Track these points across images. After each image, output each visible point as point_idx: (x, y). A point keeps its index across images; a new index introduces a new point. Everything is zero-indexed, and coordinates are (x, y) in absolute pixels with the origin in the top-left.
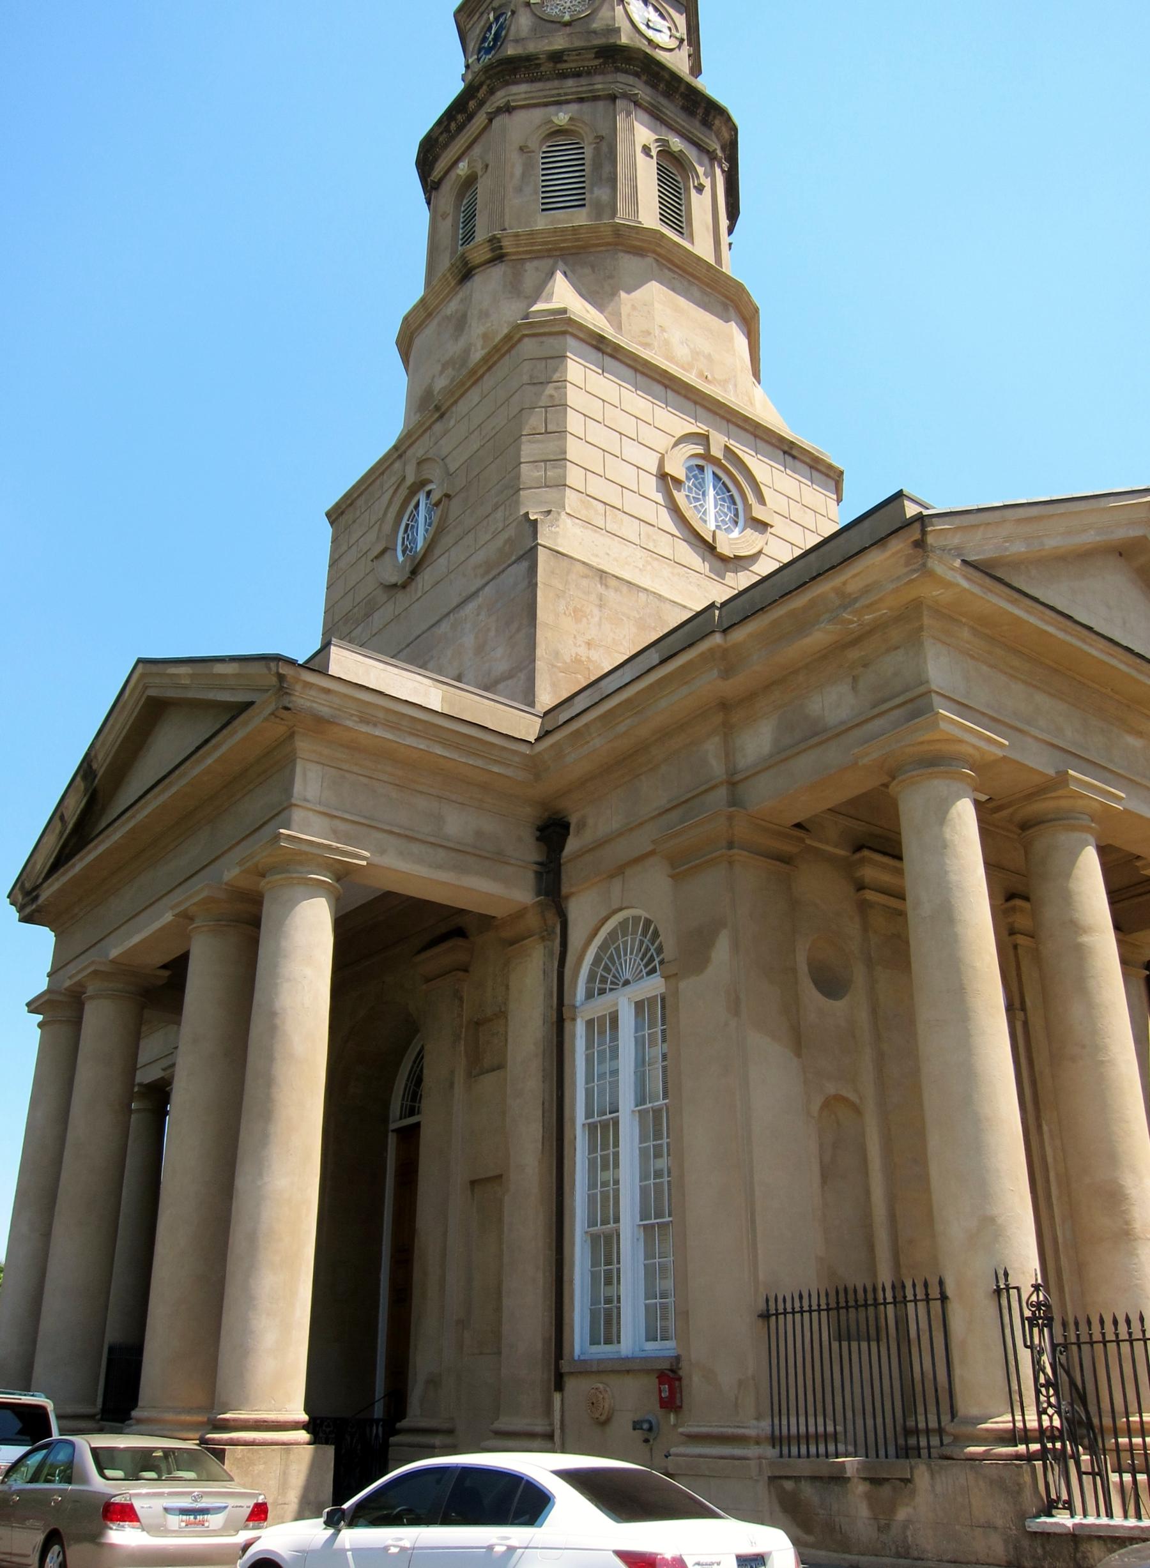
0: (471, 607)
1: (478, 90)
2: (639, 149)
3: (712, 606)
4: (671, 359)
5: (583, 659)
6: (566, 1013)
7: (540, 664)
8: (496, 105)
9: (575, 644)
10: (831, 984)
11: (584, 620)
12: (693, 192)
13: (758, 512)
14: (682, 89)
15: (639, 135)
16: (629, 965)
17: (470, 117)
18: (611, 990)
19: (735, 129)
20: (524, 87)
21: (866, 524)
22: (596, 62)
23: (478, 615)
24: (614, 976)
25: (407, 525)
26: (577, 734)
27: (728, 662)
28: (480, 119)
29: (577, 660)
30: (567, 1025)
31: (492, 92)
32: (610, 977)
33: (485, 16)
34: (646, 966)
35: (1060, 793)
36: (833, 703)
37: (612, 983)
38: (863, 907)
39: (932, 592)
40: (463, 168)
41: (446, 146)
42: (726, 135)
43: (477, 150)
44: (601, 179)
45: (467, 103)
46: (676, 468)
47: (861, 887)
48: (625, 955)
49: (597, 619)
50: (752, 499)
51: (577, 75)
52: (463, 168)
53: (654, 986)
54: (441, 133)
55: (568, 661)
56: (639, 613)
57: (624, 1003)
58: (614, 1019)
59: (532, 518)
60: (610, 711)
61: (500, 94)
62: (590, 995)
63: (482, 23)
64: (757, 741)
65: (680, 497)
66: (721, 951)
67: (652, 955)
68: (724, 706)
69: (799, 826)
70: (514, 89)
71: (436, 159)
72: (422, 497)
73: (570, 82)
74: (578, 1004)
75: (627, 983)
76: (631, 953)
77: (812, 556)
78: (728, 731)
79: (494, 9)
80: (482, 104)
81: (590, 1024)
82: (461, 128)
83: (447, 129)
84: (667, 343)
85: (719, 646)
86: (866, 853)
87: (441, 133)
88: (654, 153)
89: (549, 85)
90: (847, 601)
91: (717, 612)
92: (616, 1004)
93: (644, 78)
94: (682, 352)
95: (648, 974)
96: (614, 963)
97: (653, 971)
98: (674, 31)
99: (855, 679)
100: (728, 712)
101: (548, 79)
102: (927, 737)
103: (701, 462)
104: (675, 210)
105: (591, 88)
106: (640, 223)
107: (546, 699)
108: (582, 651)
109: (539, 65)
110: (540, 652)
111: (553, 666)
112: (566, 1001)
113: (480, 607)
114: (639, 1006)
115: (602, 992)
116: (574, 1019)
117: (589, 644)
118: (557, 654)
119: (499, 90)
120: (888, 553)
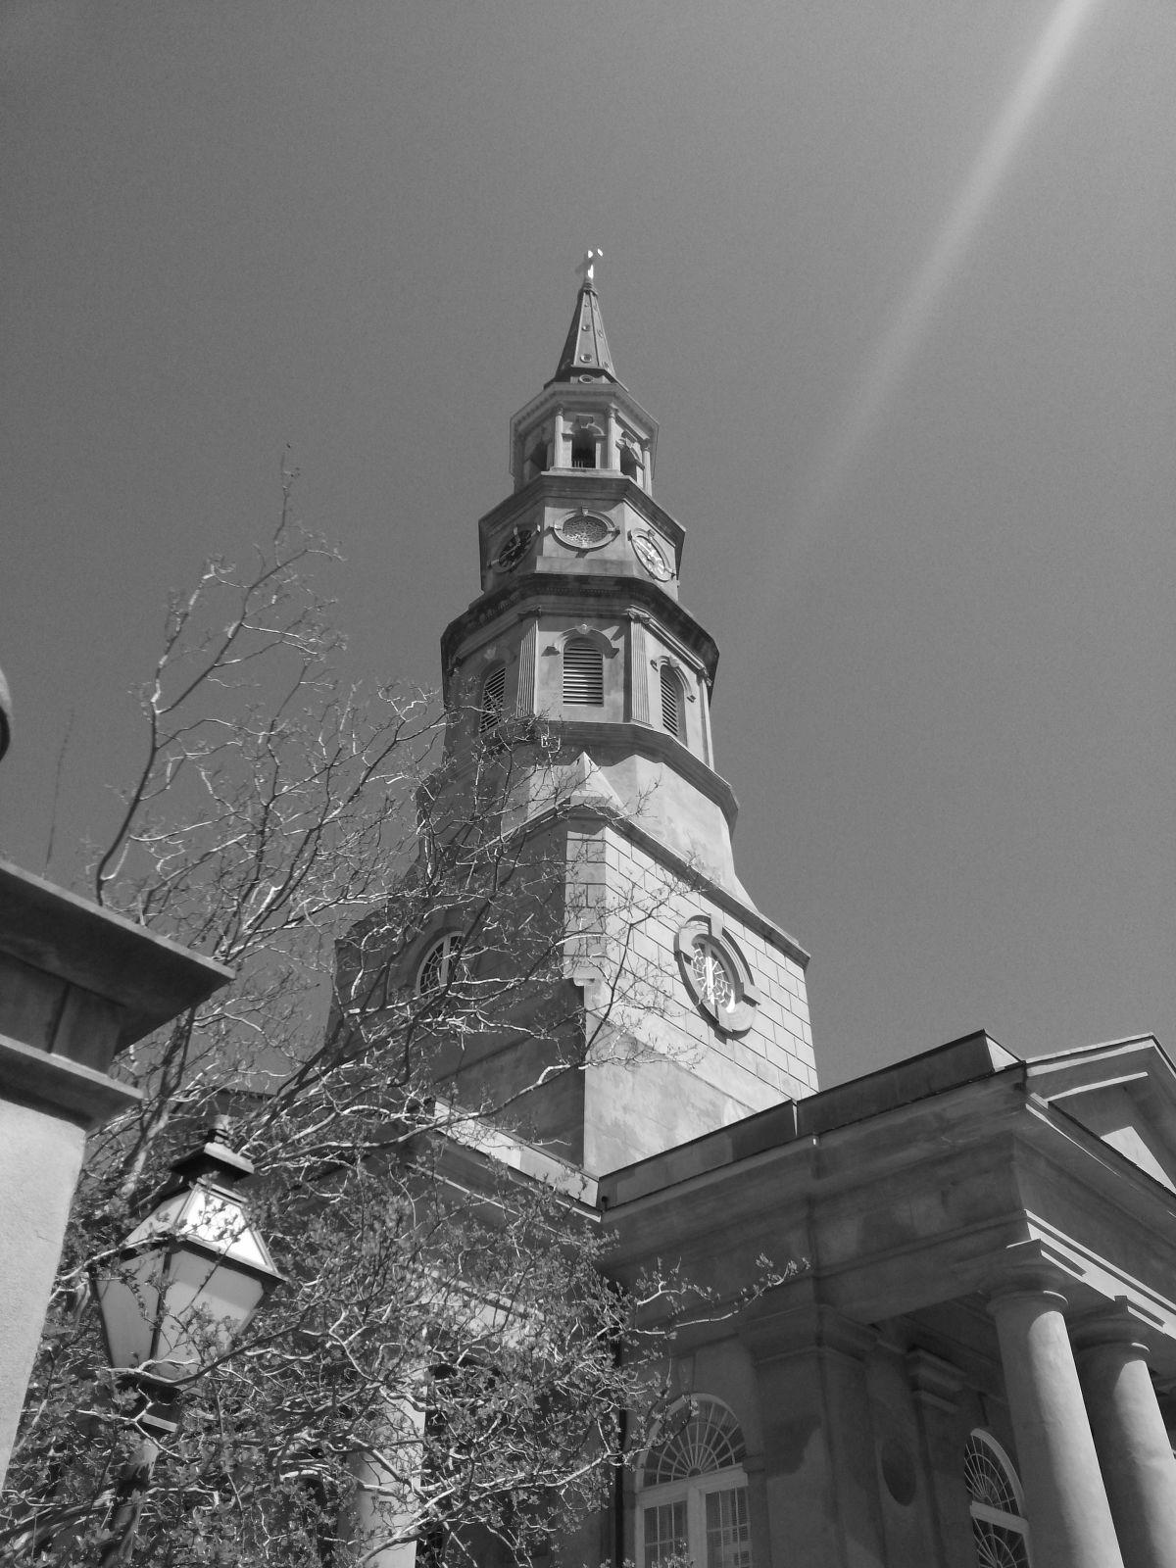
0: (508, 1059)
1: (511, 593)
2: (648, 663)
3: (789, 1103)
4: (676, 846)
5: (622, 1123)
6: (626, 1498)
7: (587, 1126)
8: (528, 609)
9: (614, 1108)
10: (902, 1491)
11: (621, 1085)
12: (686, 700)
13: (749, 991)
14: (681, 618)
15: (649, 648)
16: (698, 1451)
17: (500, 613)
18: (676, 1478)
19: (717, 654)
20: (552, 599)
21: (949, 1054)
22: (616, 588)
23: (517, 1067)
24: (680, 1463)
25: (428, 966)
26: (655, 1210)
27: (820, 1164)
28: (510, 617)
29: (616, 1124)
30: (627, 1512)
31: (523, 597)
32: (675, 1464)
33: (508, 529)
34: (719, 1456)
35: (1118, 1316)
36: (922, 1212)
37: (677, 1470)
38: (918, 1406)
39: (1023, 1128)
40: (490, 654)
41: (472, 631)
42: (710, 657)
43: (504, 641)
44: (617, 685)
45: (499, 601)
46: (687, 948)
47: (915, 1386)
48: (693, 1441)
49: (631, 1084)
50: (743, 977)
51: (598, 595)
52: (490, 654)
53: (734, 1478)
54: (470, 621)
55: (609, 1124)
56: (662, 1080)
57: (694, 1493)
58: (680, 1510)
59: (578, 984)
60: (696, 1193)
61: (531, 600)
62: (650, 1481)
63: (505, 534)
64: (843, 1239)
65: (689, 968)
66: (815, 1450)
67: (726, 1446)
68: (811, 1201)
69: (873, 1325)
70: (544, 598)
71: (461, 640)
72: (446, 942)
73: (591, 601)
74: (637, 1490)
75: (695, 1473)
76: (701, 1440)
77: (894, 1074)
78: (812, 1224)
79: (518, 526)
80: (513, 604)
81: (650, 1514)
82: (489, 620)
83: (477, 619)
84: (674, 831)
85: (815, 1147)
86: (922, 1353)
87: (470, 621)
88: (659, 668)
89: (573, 600)
90: (946, 1126)
91: (795, 1108)
92: (686, 1494)
93: (653, 606)
94: (684, 842)
95: (722, 1465)
96: (678, 1449)
97: (727, 1463)
98: (667, 567)
99: (944, 1195)
100: (813, 1209)
101: (573, 595)
102: (1028, 1262)
103: (703, 941)
104: (673, 716)
105: (610, 608)
106: (650, 725)
107: (598, 1159)
108: (619, 1115)
109: (568, 583)
110: (588, 1114)
111: (598, 1129)
112: (625, 1488)
113: (519, 1060)
114: (712, 1499)
115: (665, 1479)
116: (633, 1507)
117: (625, 1109)
118: (601, 1118)
119: (530, 596)
120: (991, 1090)
